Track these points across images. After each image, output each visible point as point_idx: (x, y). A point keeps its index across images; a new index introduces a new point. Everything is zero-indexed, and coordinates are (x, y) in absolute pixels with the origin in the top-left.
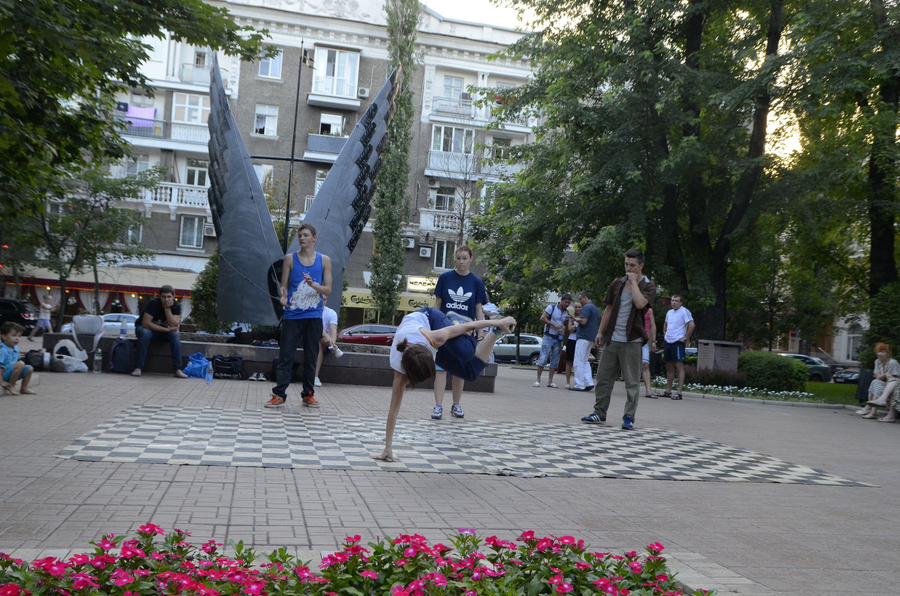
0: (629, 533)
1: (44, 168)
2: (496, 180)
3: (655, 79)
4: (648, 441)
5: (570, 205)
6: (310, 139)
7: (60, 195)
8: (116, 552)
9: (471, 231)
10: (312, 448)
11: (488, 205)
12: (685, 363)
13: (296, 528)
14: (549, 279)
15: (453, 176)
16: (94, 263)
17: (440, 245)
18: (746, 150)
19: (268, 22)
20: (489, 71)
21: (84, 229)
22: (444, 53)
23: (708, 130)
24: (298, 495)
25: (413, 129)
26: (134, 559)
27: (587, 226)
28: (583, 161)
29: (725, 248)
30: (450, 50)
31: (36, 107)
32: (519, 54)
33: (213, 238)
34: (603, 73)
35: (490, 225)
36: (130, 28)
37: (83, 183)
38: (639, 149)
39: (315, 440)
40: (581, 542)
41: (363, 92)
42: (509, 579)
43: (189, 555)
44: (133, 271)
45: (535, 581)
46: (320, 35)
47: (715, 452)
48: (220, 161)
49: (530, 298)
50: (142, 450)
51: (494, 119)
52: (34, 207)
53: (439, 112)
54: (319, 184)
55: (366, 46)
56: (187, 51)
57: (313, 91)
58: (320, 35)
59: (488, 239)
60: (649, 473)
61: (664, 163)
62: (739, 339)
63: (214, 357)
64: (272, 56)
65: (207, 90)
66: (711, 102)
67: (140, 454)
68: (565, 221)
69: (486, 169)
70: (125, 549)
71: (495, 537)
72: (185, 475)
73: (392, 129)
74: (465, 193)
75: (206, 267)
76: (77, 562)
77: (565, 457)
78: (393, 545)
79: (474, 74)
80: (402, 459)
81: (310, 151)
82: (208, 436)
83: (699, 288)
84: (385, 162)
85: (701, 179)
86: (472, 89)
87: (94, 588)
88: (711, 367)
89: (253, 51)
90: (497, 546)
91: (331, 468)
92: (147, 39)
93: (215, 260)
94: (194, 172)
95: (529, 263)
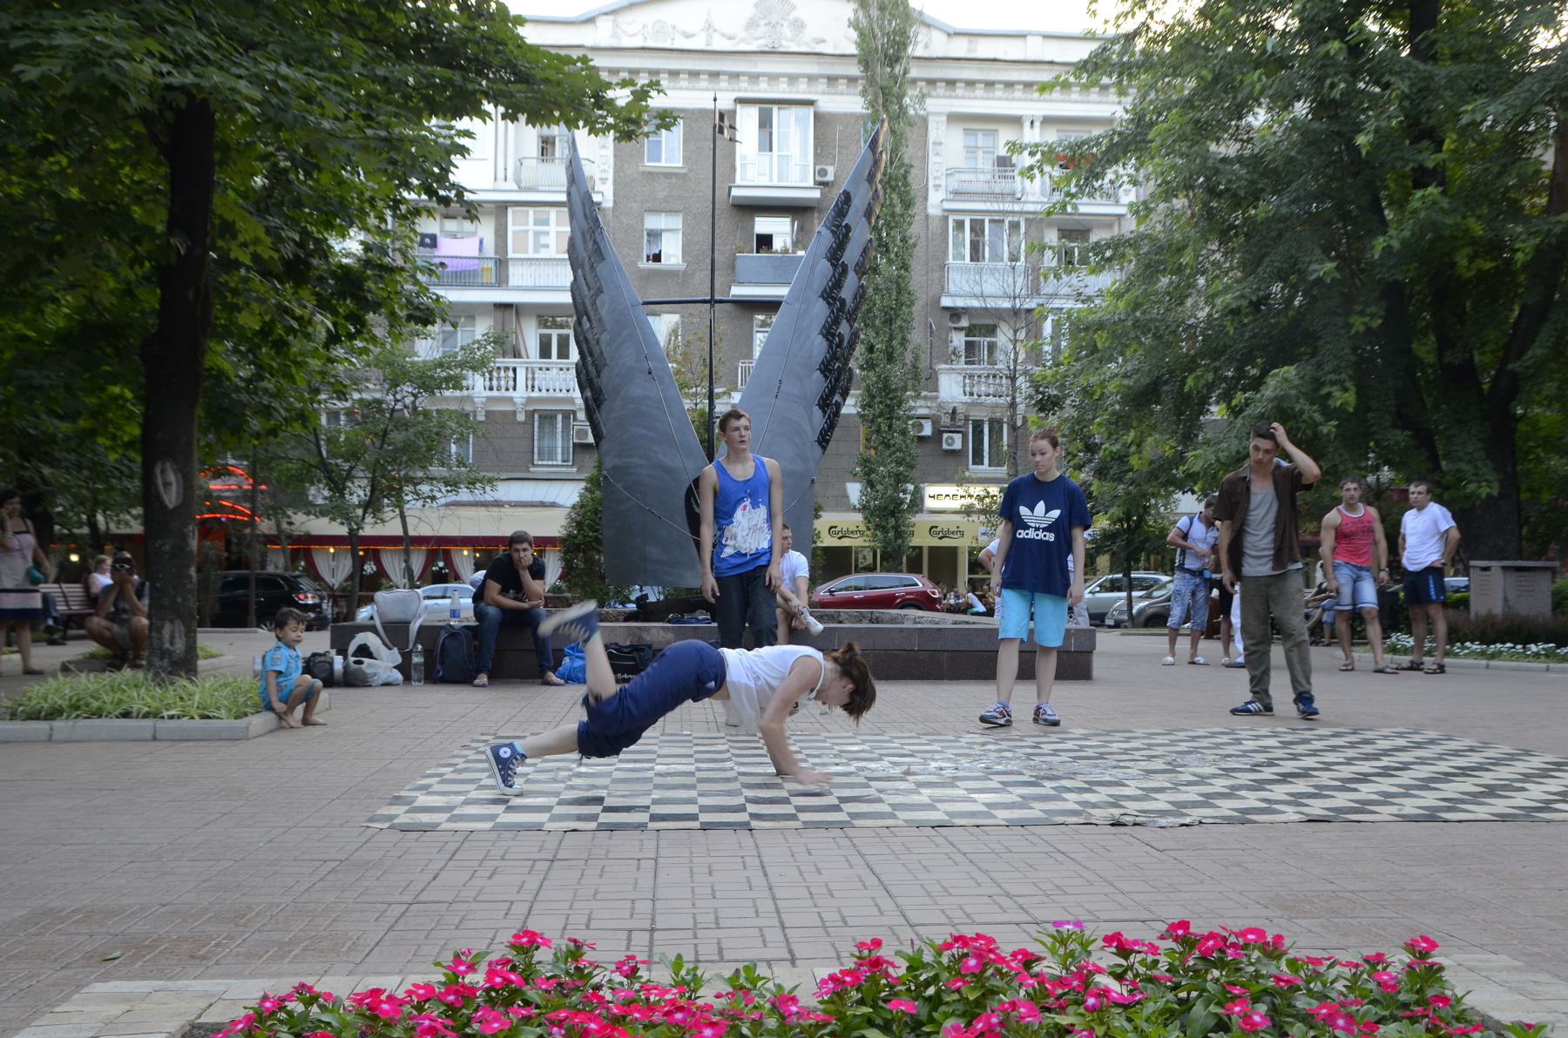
1: (314, 353)
4: (1387, 752)
6: (738, 264)
7: (342, 395)
8: (477, 978)
9: (1031, 397)
11: (1057, 349)
12: (1445, 605)
13: (758, 903)
14: (1179, 473)
15: (991, 304)
16: (400, 504)
17: (978, 426)
22: (960, 90)
24: (766, 875)
25: (915, 229)
26: (508, 989)
28: (1225, 254)
29: (1510, 387)
30: (971, 84)
32: (1094, 76)
34: (1251, 92)
35: (1063, 385)
37: (375, 373)
41: (823, 172)
42: (1150, 1007)
43: (595, 980)
44: (462, 512)
45: (1198, 1010)
47: (1521, 767)
48: (592, 314)
49: (1146, 508)
51: (1057, 197)
52: (303, 417)
53: (957, 194)
54: (759, 338)
55: (823, 93)
56: (525, 135)
57: (738, 181)
59: (1061, 408)
61: (1380, 243)
62: (1551, 555)
65: (563, 198)
66: (1465, 120)
67: (497, 816)
68: (1199, 366)
69: (1049, 286)
70: (491, 973)
74: (1015, 332)
76: (418, 996)
77: (1233, 788)
78: (940, 954)
79: (1016, 121)
80: (938, 805)
81: (741, 283)
82: (606, 781)
84: (870, 291)
85: (1453, 265)
86: (1015, 147)
88: (1498, 610)
89: (636, 122)
90: (1124, 949)
91: (817, 825)
92: (463, 123)
93: (594, 483)
95: (1139, 446)
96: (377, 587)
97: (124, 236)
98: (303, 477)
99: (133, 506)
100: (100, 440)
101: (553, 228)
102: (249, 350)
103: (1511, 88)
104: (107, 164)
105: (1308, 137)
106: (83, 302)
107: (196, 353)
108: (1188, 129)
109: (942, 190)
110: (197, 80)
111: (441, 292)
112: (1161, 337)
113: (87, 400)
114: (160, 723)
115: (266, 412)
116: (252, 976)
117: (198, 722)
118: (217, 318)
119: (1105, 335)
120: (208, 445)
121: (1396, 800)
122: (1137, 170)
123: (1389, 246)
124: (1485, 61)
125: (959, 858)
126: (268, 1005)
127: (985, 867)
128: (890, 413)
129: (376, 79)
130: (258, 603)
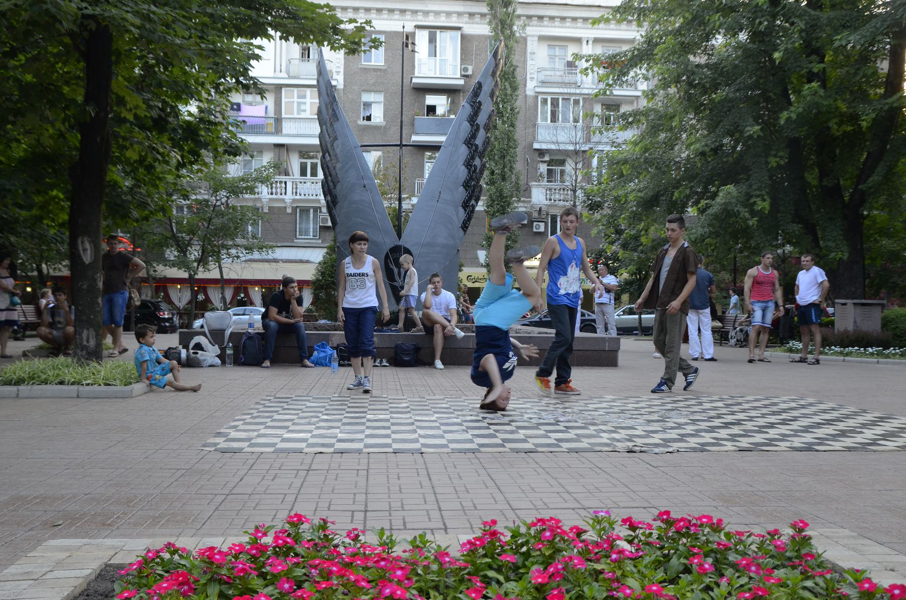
1: (170, 172)
2: (607, 148)
3: (771, 28)
4: (784, 411)
6: (417, 123)
7: (186, 197)
8: (268, 540)
9: (584, 202)
12: (821, 325)
13: (430, 512)
15: (562, 147)
16: (218, 260)
17: (554, 218)
19: (368, 10)
21: (208, 227)
22: (546, 22)
23: (835, 75)
24: (430, 480)
25: (519, 103)
26: (285, 547)
27: (706, 189)
28: (698, 121)
29: (861, 198)
30: (552, 18)
31: (160, 116)
32: (624, 16)
33: (328, 227)
34: (714, 26)
35: (603, 196)
37: (205, 184)
38: (758, 103)
39: (442, 424)
41: (466, 69)
42: (647, 559)
43: (335, 542)
44: (254, 265)
45: (674, 561)
46: (420, 17)
47: (860, 420)
48: (331, 152)
50: (277, 440)
51: (602, 86)
52: (163, 210)
53: (543, 83)
54: (428, 167)
55: (467, 23)
56: (293, 48)
57: (416, 74)
58: (420, 17)
59: (602, 209)
60: (788, 444)
61: (784, 115)
62: (882, 295)
64: (376, 48)
65: (315, 82)
66: (837, 44)
68: (682, 185)
69: (596, 138)
70: (276, 538)
71: (630, 518)
72: (320, 463)
73: (497, 104)
74: (576, 164)
75: (324, 257)
76: (235, 550)
77: (697, 431)
78: (529, 529)
79: (578, 40)
80: (529, 440)
81: (417, 134)
82: (339, 424)
85: (829, 128)
86: (578, 57)
87: (252, 575)
88: (851, 328)
89: (358, 44)
90: (633, 526)
91: (460, 451)
92: (257, 41)
95: (646, 231)
96: (206, 309)
98: (162, 244)
99: (63, 260)
101: (308, 100)
102: (132, 171)
103: (864, 25)
104: (49, 61)
105: (746, 52)
106: (34, 142)
107: (103, 172)
108: (677, 48)
109: (535, 81)
110: (102, 12)
111: (244, 137)
112: (660, 168)
114: (81, 388)
115: (143, 205)
116: (139, 536)
117: (103, 388)
118: (114, 152)
119: (628, 166)
120: (108, 226)
121: (789, 439)
122: (648, 71)
125: (540, 470)
129: (206, 14)
130: (136, 317)
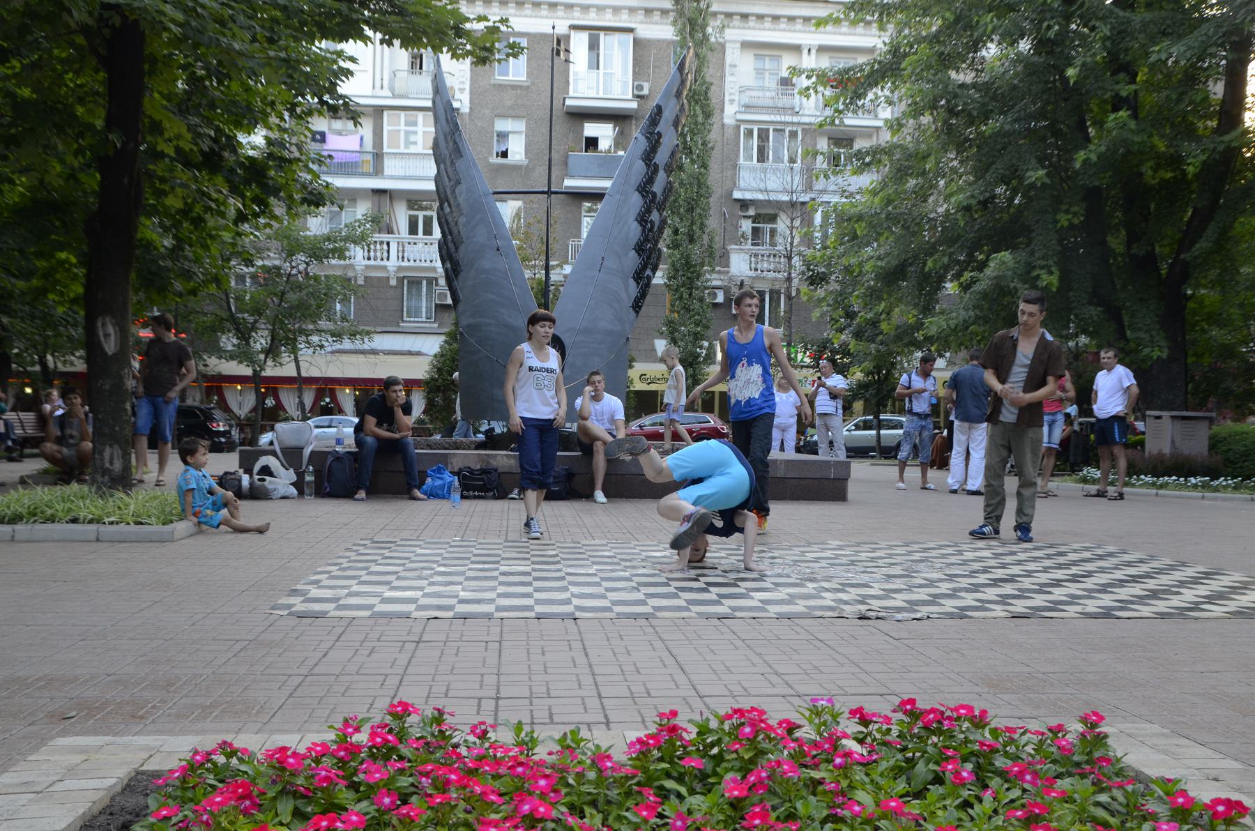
0: (1052, 697)
1: (226, 228)
2: (835, 199)
3: (1064, 31)
5: (944, 229)
6: (570, 160)
7: (249, 262)
8: (362, 738)
9: (803, 273)
10: (601, 590)
11: (825, 236)
13: (587, 700)
14: (919, 336)
15: (773, 197)
16: (294, 351)
18: (1213, 124)
20: (818, 43)
21: (280, 305)
22: (752, 22)
25: (714, 136)
26: (385, 747)
27: (970, 255)
28: (961, 162)
29: (1182, 273)
30: (760, 17)
31: (211, 149)
33: (448, 306)
34: (985, 31)
35: (829, 265)
36: (325, 35)
37: (275, 244)
38: (1044, 139)
40: (984, 713)
41: (640, 88)
42: (884, 765)
43: (455, 740)
44: (345, 358)
45: (921, 767)
48: (452, 201)
49: (893, 364)
50: (375, 600)
51: (829, 112)
52: (217, 280)
53: (748, 107)
54: (587, 223)
55: (641, 23)
56: (399, 56)
57: (571, 94)
58: (577, 13)
59: (828, 283)
60: (1079, 609)
61: (1081, 155)
62: (1210, 405)
63: (461, 470)
64: (515, 56)
65: (429, 104)
66: (1153, 58)
67: (374, 606)
69: (820, 184)
70: (373, 735)
71: (861, 708)
72: (435, 632)
73: (683, 135)
74: (792, 220)
76: (316, 752)
77: (955, 590)
78: (722, 723)
79: (796, 48)
81: (572, 177)
82: (461, 579)
83: (1142, 335)
84: (677, 185)
85: (1141, 175)
86: (795, 71)
87: (340, 786)
89: (490, 50)
90: (865, 720)
91: (629, 616)
92: (350, 47)
93: (452, 337)
94: (416, 217)
97: (69, 131)
98: (216, 328)
99: (77, 349)
100: (51, 296)
101: (420, 128)
102: (173, 226)
104: (54, 70)
105: (1029, 68)
106: (36, 183)
109: (736, 104)
111: (329, 180)
112: (908, 228)
113: (38, 263)
114: (102, 528)
115: (187, 275)
116: (183, 732)
117: (133, 528)
119: (864, 224)
120: (139, 302)
121: (1081, 601)
122: (892, 92)
123: (1088, 159)
124: (1173, 9)
125: (738, 643)
126: (198, 758)
127: (759, 651)
128: (690, 284)
